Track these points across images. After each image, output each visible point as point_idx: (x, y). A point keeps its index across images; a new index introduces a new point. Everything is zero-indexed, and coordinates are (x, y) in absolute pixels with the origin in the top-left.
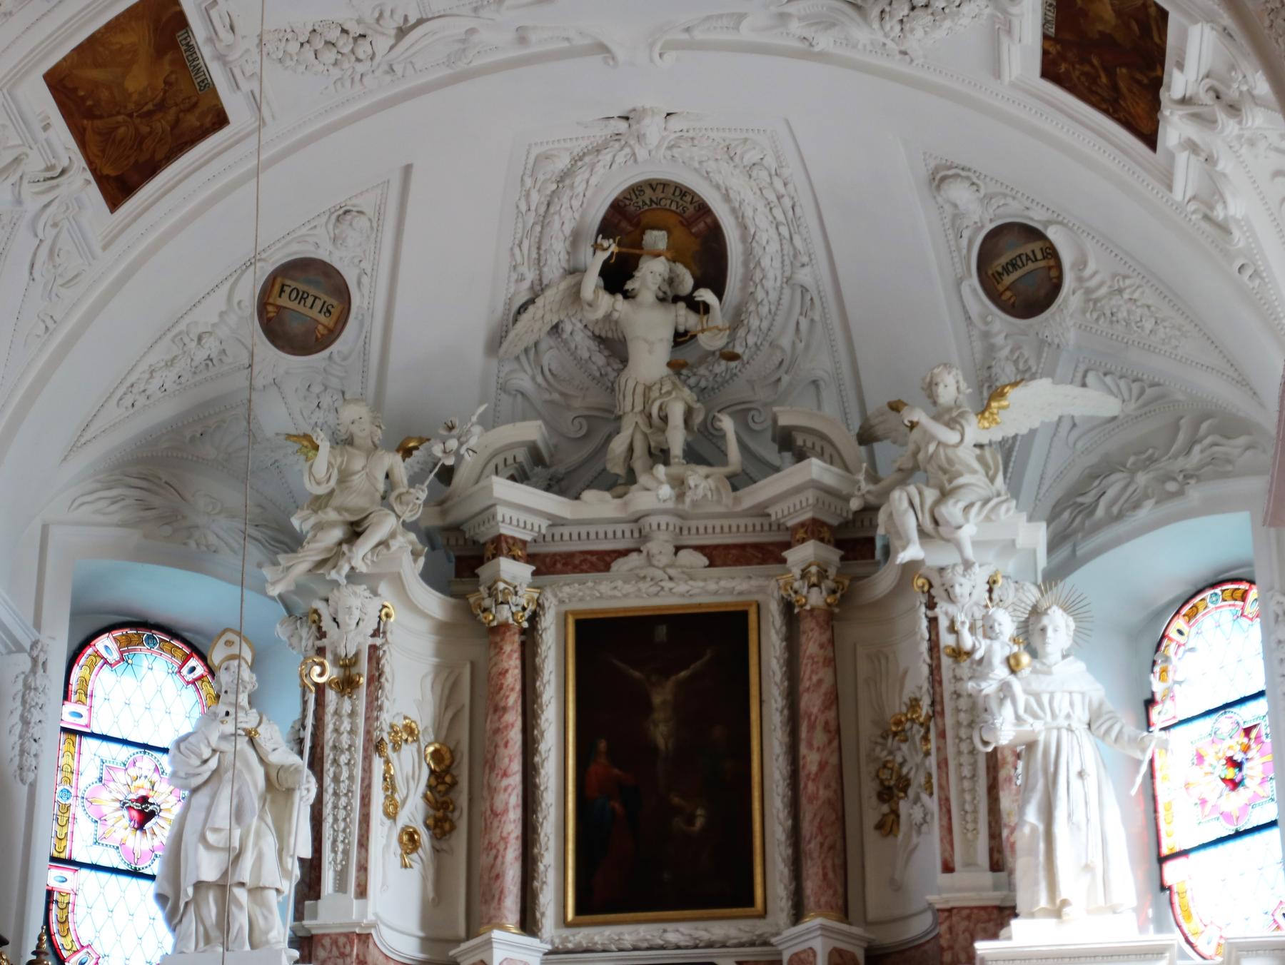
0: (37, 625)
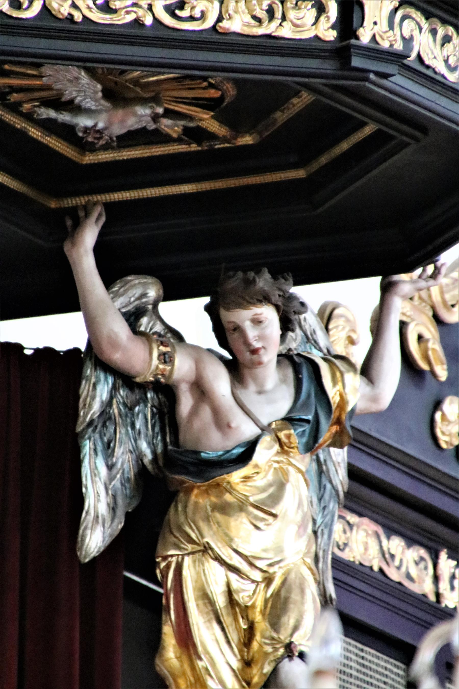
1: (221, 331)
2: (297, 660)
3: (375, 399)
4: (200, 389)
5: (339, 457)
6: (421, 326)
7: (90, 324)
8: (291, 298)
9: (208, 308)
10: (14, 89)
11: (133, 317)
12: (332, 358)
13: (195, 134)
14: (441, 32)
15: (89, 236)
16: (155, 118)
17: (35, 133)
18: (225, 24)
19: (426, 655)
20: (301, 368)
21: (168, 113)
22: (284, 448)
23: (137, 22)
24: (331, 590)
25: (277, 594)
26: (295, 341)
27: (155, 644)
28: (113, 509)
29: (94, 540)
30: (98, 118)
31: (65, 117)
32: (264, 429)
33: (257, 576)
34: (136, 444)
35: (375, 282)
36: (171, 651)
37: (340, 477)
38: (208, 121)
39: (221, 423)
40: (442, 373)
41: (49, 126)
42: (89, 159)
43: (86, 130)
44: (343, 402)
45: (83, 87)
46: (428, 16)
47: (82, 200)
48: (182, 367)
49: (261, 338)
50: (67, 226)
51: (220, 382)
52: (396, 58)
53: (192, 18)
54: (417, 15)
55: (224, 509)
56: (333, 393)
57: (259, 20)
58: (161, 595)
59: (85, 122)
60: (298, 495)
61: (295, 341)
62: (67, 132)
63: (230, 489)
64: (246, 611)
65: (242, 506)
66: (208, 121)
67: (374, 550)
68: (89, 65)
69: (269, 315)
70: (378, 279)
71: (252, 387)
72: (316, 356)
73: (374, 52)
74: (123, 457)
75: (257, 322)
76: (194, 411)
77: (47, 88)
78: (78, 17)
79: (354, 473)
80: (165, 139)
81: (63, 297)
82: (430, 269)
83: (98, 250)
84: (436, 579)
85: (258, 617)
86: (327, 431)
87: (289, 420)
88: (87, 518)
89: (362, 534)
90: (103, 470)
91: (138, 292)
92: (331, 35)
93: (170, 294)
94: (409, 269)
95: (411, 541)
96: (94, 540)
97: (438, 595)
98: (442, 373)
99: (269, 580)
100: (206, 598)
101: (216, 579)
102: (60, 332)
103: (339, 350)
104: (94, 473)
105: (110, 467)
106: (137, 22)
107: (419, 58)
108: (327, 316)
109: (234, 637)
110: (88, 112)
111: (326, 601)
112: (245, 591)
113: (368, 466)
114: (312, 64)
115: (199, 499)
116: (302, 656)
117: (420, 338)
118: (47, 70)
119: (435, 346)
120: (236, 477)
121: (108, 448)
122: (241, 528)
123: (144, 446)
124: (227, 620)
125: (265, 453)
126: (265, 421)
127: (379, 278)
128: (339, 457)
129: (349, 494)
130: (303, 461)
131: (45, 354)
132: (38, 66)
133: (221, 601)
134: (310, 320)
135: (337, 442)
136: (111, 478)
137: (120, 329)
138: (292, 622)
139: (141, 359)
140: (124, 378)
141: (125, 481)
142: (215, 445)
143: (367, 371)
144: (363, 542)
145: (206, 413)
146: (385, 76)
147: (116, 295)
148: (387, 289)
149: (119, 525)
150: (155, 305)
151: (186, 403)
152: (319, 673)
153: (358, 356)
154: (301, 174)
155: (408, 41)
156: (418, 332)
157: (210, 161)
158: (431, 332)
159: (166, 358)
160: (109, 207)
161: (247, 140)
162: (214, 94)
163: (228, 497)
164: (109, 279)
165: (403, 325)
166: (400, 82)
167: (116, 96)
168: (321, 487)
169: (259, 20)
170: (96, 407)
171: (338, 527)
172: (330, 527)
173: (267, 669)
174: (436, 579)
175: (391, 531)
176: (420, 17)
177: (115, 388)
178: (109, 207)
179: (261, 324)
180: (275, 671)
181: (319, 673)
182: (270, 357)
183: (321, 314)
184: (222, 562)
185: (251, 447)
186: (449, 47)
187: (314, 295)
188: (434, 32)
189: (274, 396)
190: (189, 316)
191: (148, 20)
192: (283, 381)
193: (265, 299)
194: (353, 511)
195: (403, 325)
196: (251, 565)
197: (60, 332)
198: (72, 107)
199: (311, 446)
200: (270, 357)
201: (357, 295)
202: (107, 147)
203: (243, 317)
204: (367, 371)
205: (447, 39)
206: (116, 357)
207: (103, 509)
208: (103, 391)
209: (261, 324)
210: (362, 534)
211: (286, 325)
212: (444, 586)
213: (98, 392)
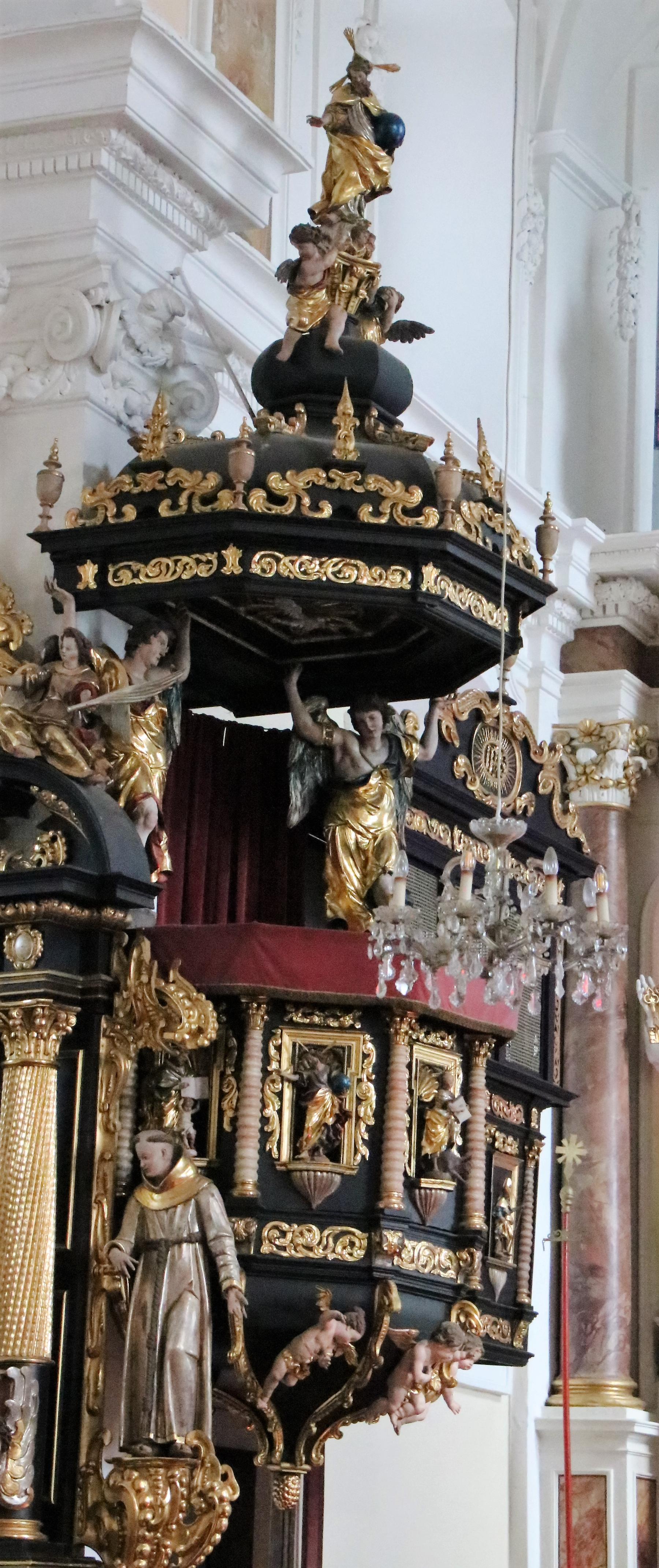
0: (629, 178)
1: (355, 722)
2: (388, 875)
3: (426, 755)
4: (345, 749)
5: (409, 781)
6: (448, 722)
7: (295, 719)
8: (389, 708)
9: (349, 712)
10: (262, 609)
11: (314, 715)
12: (406, 735)
13: (345, 631)
14: (458, 587)
15: (295, 678)
16: (327, 623)
17: (271, 629)
18: (360, 581)
19: (448, 871)
20: (393, 741)
21: (333, 621)
22: (383, 778)
23: (319, 579)
24: (404, 843)
25: (379, 844)
26: (389, 727)
27: (323, 867)
28: (303, 804)
29: (295, 818)
30: (300, 623)
31: (285, 622)
32: (375, 768)
33: (370, 836)
34: (314, 775)
35: (426, 701)
36: (329, 870)
37: (409, 790)
38: (350, 625)
39: (354, 764)
40: (457, 744)
41: (278, 627)
42: (296, 642)
43: (294, 628)
44: (411, 756)
45: (293, 608)
46: (452, 579)
47: (289, 661)
48: (337, 738)
49: (374, 726)
50: (286, 673)
51: (355, 748)
52: (438, 598)
53: (344, 578)
54: (447, 579)
55: (356, 805)
56: (407, 752)
57: (375, 580)
58: (324, 845)
59: (294, 625)
60: (389, 800)
61: (389, 727)
62: (286, 629)
63: (359, 796)
64: (365, 852)
65: (363, 804)
66: (350, 625)
67: (424, 825)
68: (298, 599)
69: (378, 715)
70: (428, 700)
71: (369, 749)
72: (399, 734)
73: (428, 595)
74: (308, 779)
75: (372, 718)
76: (342, 759)
77: (276, 609)
78: (292, 576)
79: (415, 789)
80: (331, 633)
81: (281, 706)
82: (452, 696)
83: (299, 684)
84: (452, 839)
85: (370, 855)
86: (404, 770)
87: (386, 764)
88: (292, 808)
89: (418, 818)
90: (299, 786)
91: (316, 704)
92: (408, 587)
93: (332, 705)
94: (443, 695)
95: (441, 821)
96: (295, 818)
97: (453, 846)
98: (457, 744)
99: (375, 838)
100: (346, 846)
101: (351, 836)
102: (282, 721)
103: (410, 732)
104: (295, 787)
105: (303, 784)
106: (319, 579)
107: (448, 598)
108: (405, 716)
109: (358, 864)
110: (296, 620)
111: (401, 847)
112: (364, 842)
113: (421, 785)
114: (400, 601)
115: (344, 801)
116: (391, 873)
117: (447, 727)
118: (278, 601)
119: (454, 731)
120: (361, 790)
121: (302, 778)
122: (363, 813)
123: (319, 775)
124: (356, 856)
125: (373, 781)
126: (375, 764)
127: (428, 700)
128: (409, 781)
129: (413, 799)
130: (391, 784)
131: (274, 732)
132: (273, 599)
133: (353, 847)
134: (397, 718)
135: (408, 775)
136: (303, 790)
137: (308, 720)
138: (386, 857)
139: (318, 735)
140: (310, 744)
141: (310, 792)
142: (352, 775)
143: (423, 742)
144: (419, 822)
145: (348, 761)
146: (432, 606)
147: (306, 705)
148: (432, 704)
149: (306, 812)
150: (325, 709)
151: (338, 756)
152: (398, 879)
153: (419, 734)
154: (392, 650)
155: (443, 591)
156: (306, 119)
157: (350, 643)
158: (452, 725)
159: (330, 735)
160: (306, 665)
161: (370, 634)
162: (353, 612)
163: (357, 800)
164: (303, 698)
165: (440, 722)
166: (439, 608)
167: (310, 612)
168: (400, 796)
169: (375, 580)
170: (297, 756)
171: (408, 814)
172: (404, 814)
173: (374, 879)
174: (452, 839)
175: (432, 817)
176: (28, 1398)
177: (304, 750)
178: (306, 665)
179: (375, 720)
180: (377, 880)
181: (398, 879)
182: (378, 735)
183: (401, 716)
184: (353, 829)
185: (368, 777)
186: (462, 595)
187: (398, 706)
188: (455, 587)
189: (379, 755)
190: (340, 715)
191: (324, 579)
192: (383, 746)
193: (375, 708)
194: (415, 807)
195: (440, 722)
196: (368, 831)
197: (282, 721)
198: (291, 619)
199: (396, 777)
200: (378, 735)
201: (418, 707)
202: (304, 636)
203: (366, 716)
204: (423, 742)
205: (461, 591)
206: (307, 733)
207: (299, 803)
208: (300, 750)
209: (375, 720)
210: (418, 818)
211: (386, 720)
212: (456, 842)
213: (298, 750)
